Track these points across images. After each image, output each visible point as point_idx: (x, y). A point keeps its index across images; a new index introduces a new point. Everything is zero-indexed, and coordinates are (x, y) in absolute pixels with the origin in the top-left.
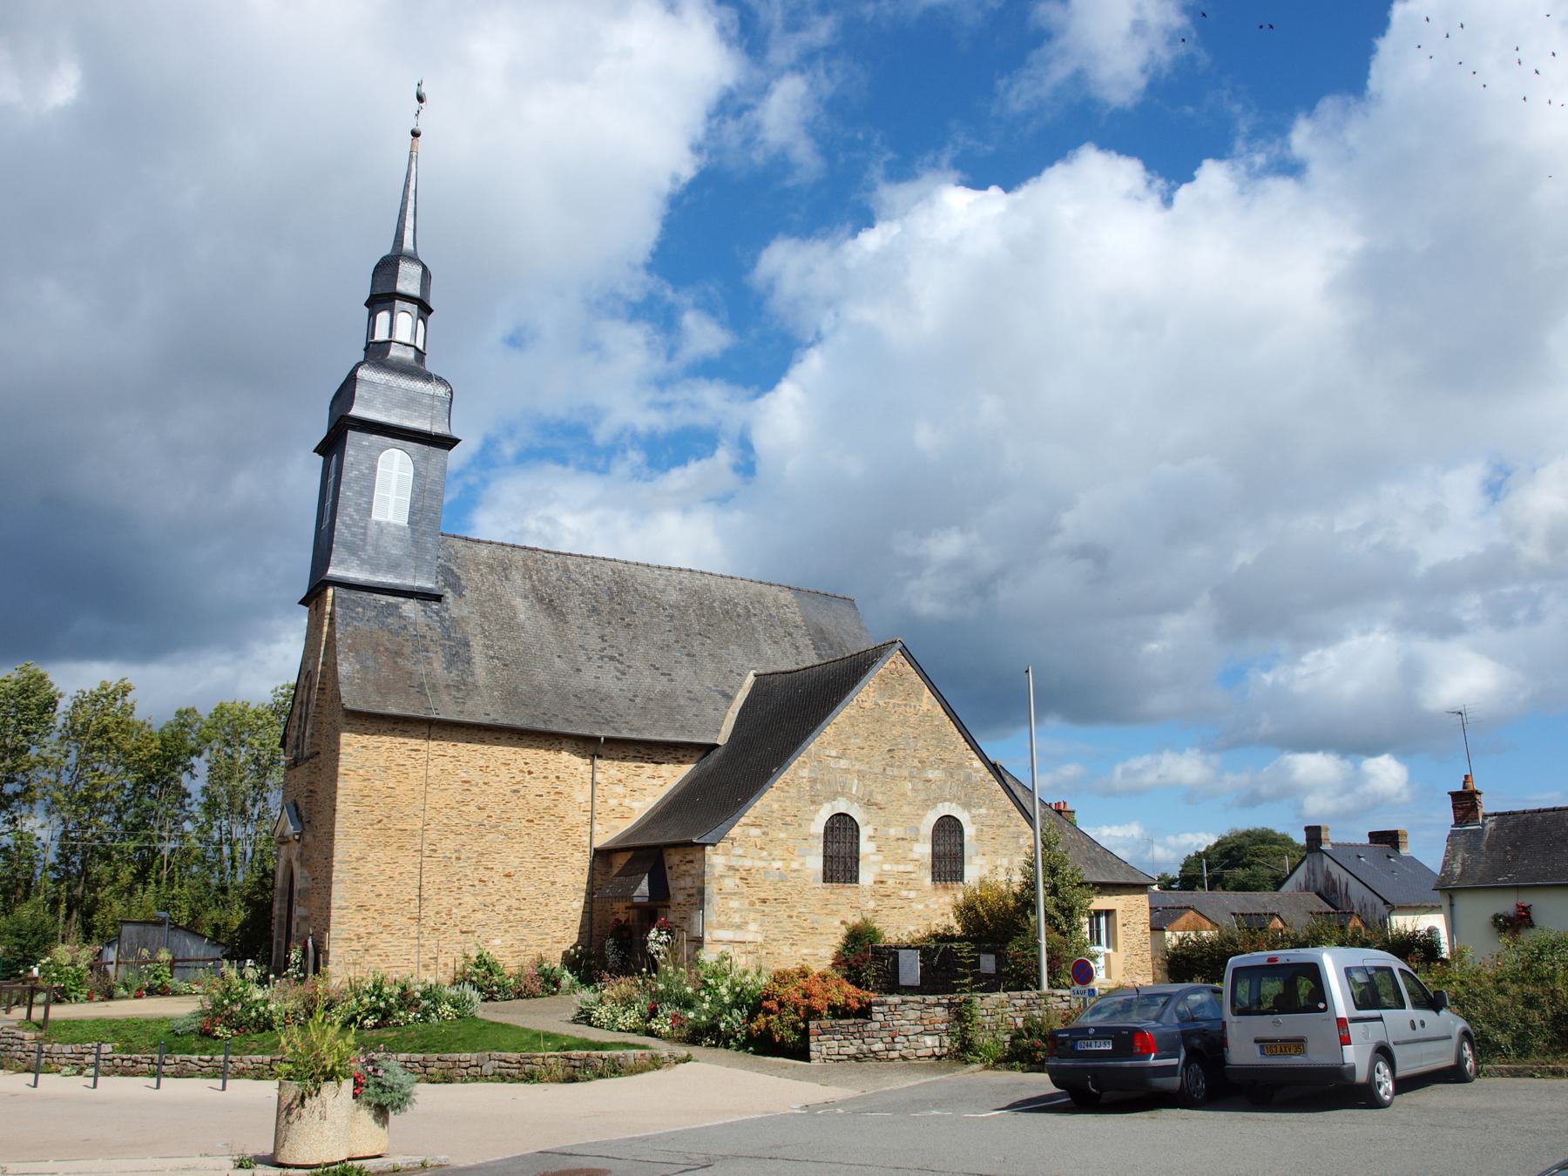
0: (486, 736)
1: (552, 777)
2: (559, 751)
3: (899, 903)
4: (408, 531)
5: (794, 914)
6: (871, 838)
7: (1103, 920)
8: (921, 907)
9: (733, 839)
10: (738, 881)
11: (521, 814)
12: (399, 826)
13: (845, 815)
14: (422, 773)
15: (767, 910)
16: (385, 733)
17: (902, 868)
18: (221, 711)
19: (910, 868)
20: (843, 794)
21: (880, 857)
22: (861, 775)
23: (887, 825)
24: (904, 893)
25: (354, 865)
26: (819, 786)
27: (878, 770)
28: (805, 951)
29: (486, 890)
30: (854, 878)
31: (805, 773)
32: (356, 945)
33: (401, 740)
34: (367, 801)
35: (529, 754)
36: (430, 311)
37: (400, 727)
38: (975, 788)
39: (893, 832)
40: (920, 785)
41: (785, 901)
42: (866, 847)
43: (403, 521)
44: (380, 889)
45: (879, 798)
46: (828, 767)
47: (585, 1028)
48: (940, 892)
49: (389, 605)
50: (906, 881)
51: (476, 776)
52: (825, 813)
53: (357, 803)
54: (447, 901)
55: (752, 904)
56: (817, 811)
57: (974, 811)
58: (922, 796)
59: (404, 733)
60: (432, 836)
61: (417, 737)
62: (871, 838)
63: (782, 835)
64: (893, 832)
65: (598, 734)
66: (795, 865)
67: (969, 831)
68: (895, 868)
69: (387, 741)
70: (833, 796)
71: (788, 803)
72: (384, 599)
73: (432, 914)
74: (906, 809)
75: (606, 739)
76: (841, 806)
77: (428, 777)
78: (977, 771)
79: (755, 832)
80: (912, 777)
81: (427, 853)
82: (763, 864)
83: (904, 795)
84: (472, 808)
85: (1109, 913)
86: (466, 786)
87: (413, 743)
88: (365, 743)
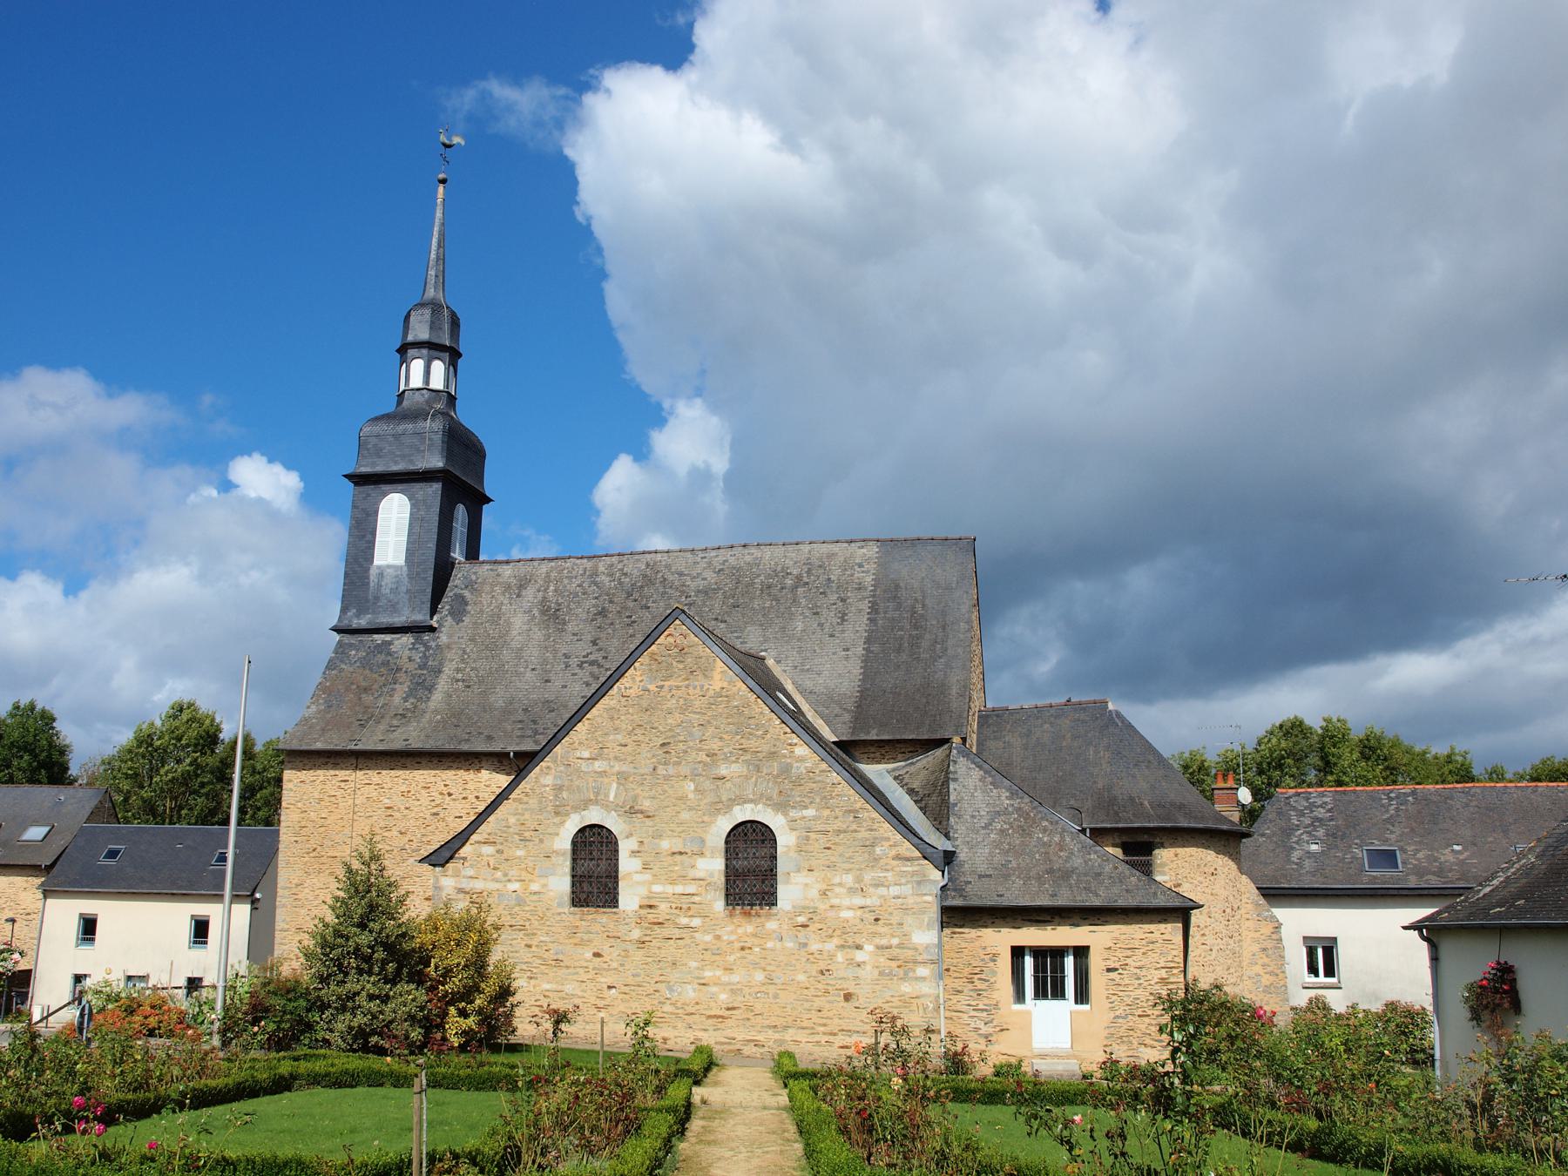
1: (471, 798)
2: (478, 770)
3: (677, 933)
5: (534, 943)
6: (634, 853)
7: (1069, 962)
8: (708, 938)
9: (464, 859)
13: (582, 830)
16: (319, 768)
17: (679, 889)
19: (691, 889)
20: (596, 802)
21: (647, 876)
22: (622, 778)
23: (658, 836)
24: (684, 921)
27: (649, 770)
28: (548, 986)
31: (548, 780)
33: (332, 772)
38: (798, 782)
39: (665, 845)
41: (523, 928)
42: (627, 864)
45: (646, 804)
46: (578, 770)
47: (485, 1056)
49: (384, 642)
50: (685, 904)
51: (399, 802)
56: (563, 823)
57: (793, 814)
58: (710, 798)
59: (336, 766)
61: (347, 769)
62: (634, 853)
63: (520, 853)
64: (665, 845)
65: (509, 749)
66: (535, 887)
67: (785, 840)
68: (670, 889)
69: (321, 774)
70: (585, 805)
71: (527, 816)
72: (379, 638)
74: (685, 815)
75: (516, 753)
76: (594, 816)
78: (801, 759)
79: (488, 850)
80: (694, 776)
83: (683, 798)
85: (1081, 952)
87: (343, 774)
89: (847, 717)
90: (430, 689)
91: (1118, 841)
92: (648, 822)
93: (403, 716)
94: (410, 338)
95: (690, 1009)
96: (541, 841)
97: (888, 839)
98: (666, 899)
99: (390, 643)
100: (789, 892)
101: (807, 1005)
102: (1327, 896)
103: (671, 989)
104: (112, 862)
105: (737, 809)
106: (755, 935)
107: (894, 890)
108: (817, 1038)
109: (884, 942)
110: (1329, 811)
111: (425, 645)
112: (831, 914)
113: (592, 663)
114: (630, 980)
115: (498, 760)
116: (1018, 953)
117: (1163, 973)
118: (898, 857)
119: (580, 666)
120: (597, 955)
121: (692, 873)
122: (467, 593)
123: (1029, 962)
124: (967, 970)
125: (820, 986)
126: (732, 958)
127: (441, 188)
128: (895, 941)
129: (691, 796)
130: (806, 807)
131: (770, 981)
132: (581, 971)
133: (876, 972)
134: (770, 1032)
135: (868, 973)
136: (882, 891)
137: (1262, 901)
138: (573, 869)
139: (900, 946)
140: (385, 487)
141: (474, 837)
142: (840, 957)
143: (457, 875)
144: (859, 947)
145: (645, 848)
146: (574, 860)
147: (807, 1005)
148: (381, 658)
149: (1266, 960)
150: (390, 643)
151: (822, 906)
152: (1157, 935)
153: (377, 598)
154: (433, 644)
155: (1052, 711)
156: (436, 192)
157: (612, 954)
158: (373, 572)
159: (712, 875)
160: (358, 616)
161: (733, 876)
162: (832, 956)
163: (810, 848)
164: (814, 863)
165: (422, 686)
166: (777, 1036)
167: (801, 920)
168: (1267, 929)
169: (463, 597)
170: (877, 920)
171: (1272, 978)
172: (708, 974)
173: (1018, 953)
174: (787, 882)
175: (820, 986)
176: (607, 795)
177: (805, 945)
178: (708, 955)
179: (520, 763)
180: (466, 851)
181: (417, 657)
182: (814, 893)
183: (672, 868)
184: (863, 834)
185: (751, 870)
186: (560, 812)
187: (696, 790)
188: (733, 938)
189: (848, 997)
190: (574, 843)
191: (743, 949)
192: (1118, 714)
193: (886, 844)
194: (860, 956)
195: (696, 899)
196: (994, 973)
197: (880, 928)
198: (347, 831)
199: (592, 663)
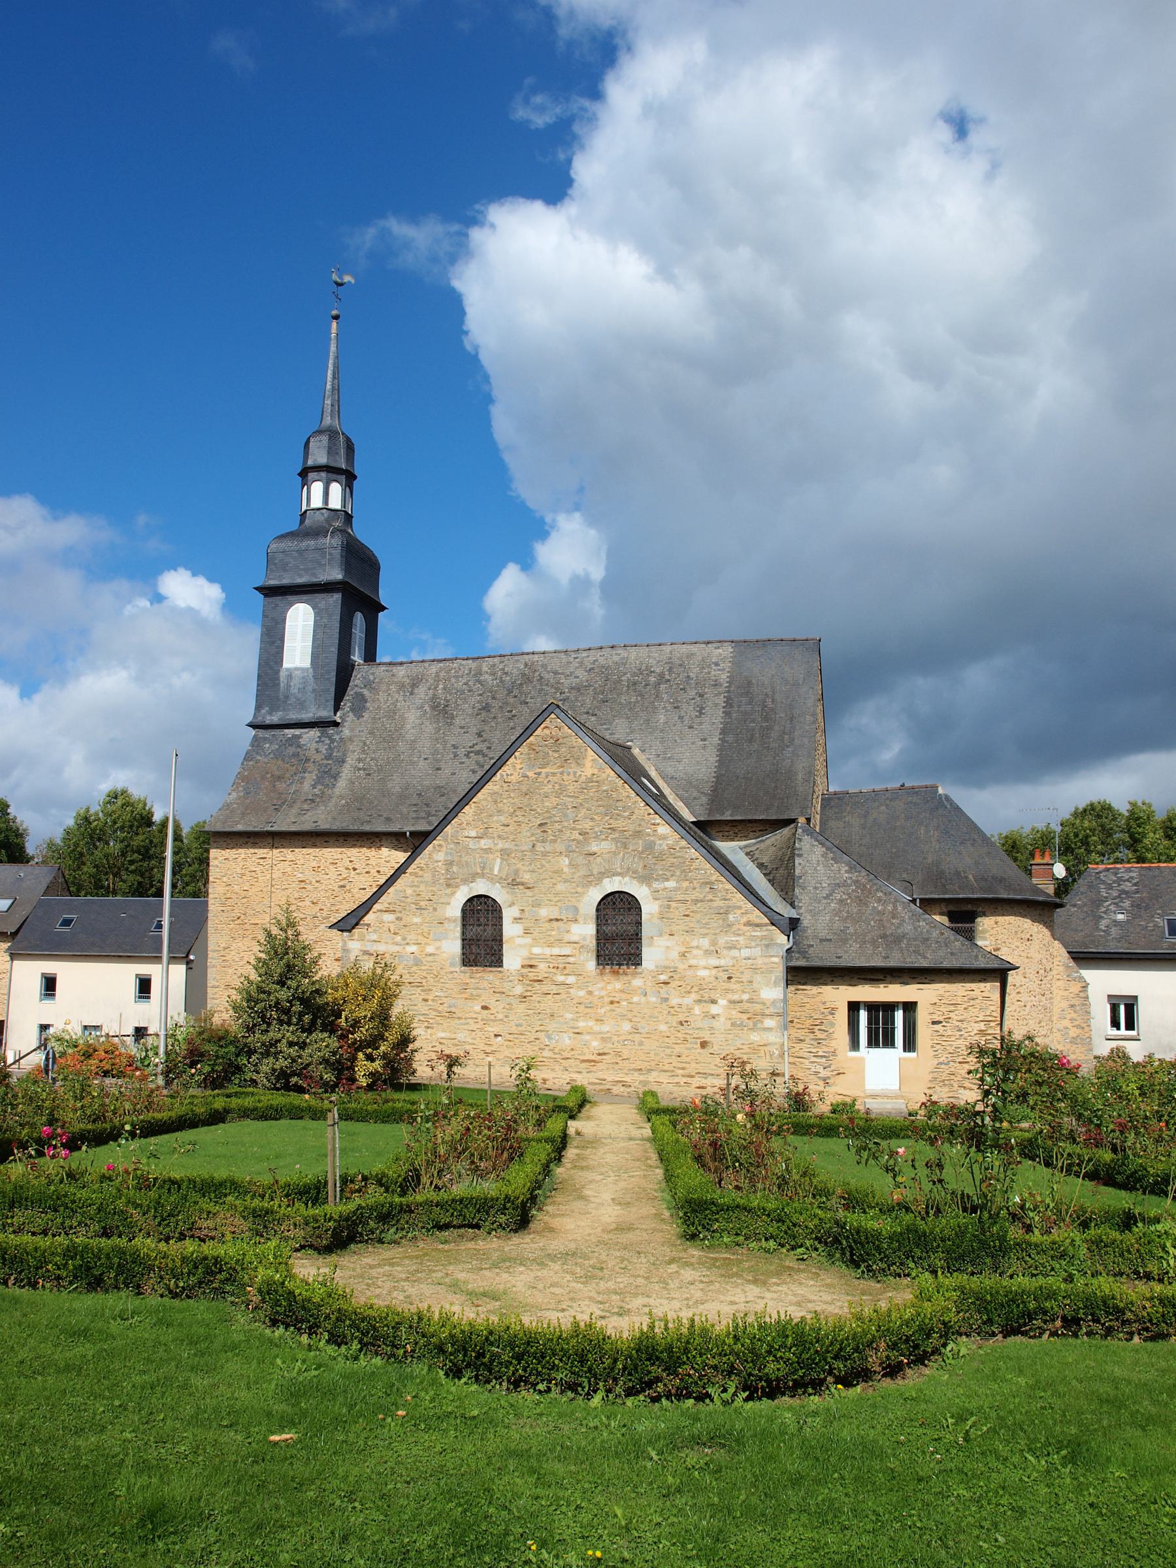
0: (318, 841)
1: (373, 872)
2: (379, 848)
3: (554, 989)
6: (517, 920)
7: (899, 1015)
9: (368, 925)
13: (470, 900)
16: (241, 847)
20: (483, 876)
21: (528, 940)
22: (505, 853)
24: (560, 978)
25: (222, 953)
26: (455, 869)
27: (528, 847)
28: (442, 1035)
30: (634, 959)
31: (440, 856)
33: (252, 851)
34: (229, 902)
35: (353, 853)
36: (355, 477)
37: (252, 840)
38: (660, 857)
39: (544, 912)
40: (581, 860)
41: (420, 985)
42: (510, 929)
45: (526, 877)
46: (467, 848)
47: (390, 1094)
49: (294, 736)
50: (562, 965)
51: (309, 875)
52: (462, 895)
53: (223, 904)
56: (453, 893)
57: (656, 885)
58: (583, 871)
62: (517, 920)
63: (417, 920)
64: (544, 912)
66: (430, 949)
67: (649, 909)
68: (548, 951)
69: (242, 852)
70: (472, 878)
71: (422, 887)
72: (289, 732)
74: (560, 887)
75: (412, 833)
77: (272, 879)
78: (664, 838)
80: (569, 852)
82: (397, 948)
83: (559, 872)
85: (910, 1007)
86: (303, 885)
87: (261, 852)
88: (227, 856)
89: (704, 800)
93: (312, 801)
94: (310, 463)
95: (566, 1055)
96: (435, 909)
98: (544, 960)
99: (299, 737)
100: (652, 954)
101: (668, 1051)
103: (549, 1038)
104: (66, 929)
105: (606, 881)
106: (622, 991)
107: (745, 953)
108: (676, 1080)
109: (736, 997)
110: (1135, 885)
111: (330, 738)
112: (689, 973)
113: (477, 753)
114: (514, 1030)
115: (396, 839)
116: (854, 1007)
117: (982, 1026)
118: (748, 924)
119: (467, 756)
120: (485, 1008)
121: (567, 937)
122: (366, 692)
123: (863, 1015)
124: (809, 1022)
125: (679, 1035)
126: (603, 1011)
127: (334, 324)
128: (745, 997)
130: (667, 880)
131: (636, 1030)
133: (729, 1022)
134: (636, 1074)
135: (721, 1024)
137: (1072, 964)
138: (463, 933)
139: (750, 1001)
140: (290, 598)
141: (376, 907)
142: (697, 1010)
144: (714, 1002)
145: (527, 915)
146: (464, 926)
147: (668, 1051)
148: (291, 750)
149: (1074, 1015)
150: (299, 737)
151: (681, 966)
153: (287, 697)
154: (337, 737)
155: (888, 795)
157: (497, 1007)
158: (283, 674)
159: (584, 939)
161: (602, 939)
162: (690, 1010)
163: (669, 915)
164: (674, 928)
165: (328, 775)
167: (663, 978)
168: (1075, 988)
169: (363, 695)
170: (730, 978)
171: (1079, 1031)
172: (581, 1024)
173: (854, 1007)
174: (651, 945)
175: (679, 1035)
176: (492, 869)
177: (667, 1000)
178: (581, 1008)
179: (416, 842)
180: (370, 918)
182: (674, 954)
183: (549, 933)
184: (719, 903)
185: (619, 934)
188: (604, 993)
189: (704, 1045)
190: (464, 911)
191: (612, 1003)
192: (947, 798)
193: (739, 912)
194: (714, 1010)
195: (571, 960)
196: (832, 1025)
197: (732, 985)
198: (266, 902)
199: (477, 753)
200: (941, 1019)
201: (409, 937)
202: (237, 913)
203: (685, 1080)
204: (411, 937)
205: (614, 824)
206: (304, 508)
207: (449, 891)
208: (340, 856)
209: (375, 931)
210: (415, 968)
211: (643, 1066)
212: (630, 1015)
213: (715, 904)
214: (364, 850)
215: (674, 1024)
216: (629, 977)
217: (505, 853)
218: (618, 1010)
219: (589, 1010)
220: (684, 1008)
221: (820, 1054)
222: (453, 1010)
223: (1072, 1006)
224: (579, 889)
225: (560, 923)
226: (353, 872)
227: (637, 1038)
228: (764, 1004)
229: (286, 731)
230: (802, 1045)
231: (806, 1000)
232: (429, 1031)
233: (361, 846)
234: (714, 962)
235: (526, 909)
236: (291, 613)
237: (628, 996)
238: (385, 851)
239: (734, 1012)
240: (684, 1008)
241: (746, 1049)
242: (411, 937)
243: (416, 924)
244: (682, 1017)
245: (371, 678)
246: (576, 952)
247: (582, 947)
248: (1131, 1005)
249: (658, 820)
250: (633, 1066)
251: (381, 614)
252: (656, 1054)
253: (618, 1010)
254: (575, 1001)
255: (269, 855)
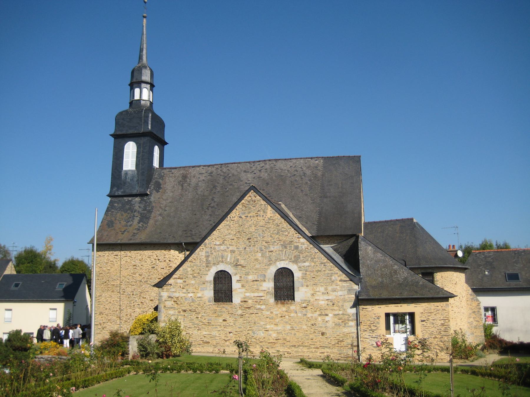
1: (167, 261)
2: (170, 250)
3: (256, 311)
4: (136, 171)
5: (199, 316)
9: (171, 285)
10: (173, 303)
11: (155, 276)
12: (112, 284)
14: (119, 263)
15: (186, 315)
17: (256, 294)
18: (25, 251)
19: (261, 294)
20: (222, 262)
21: (244, 290)
23: (247, 274)
24: (258, 307)
28: (205, 333)
29: (144, 306)
30: (292, 298)
32: (99, 327)
33: (112, 252)
34: (101, 275)
35: (158, 252)
38: (301, 252)
41: (195, 311)
42: (235, 285)
43: (134, 168)
44: (107, 307)
45: (242, 262)
48: (280, 305)
50: (259, 300)
51: (138, 263)
52: (213, 271)
54: (130, 311)
55: (179, 312)
56: (209, 270)
57: (299, 264)
59: (113, 250)
60: (123, 286)
63: (193, 282)
66: (199, 295)
67: (297, 275)
68: (252, 295)
71: (195, 268)
73: (125, 315)
75: (185, 244)
76: (221, 267)
79: (180, 281)
81: (122, 293)
83: (256, 260)
84: (137, 275)
85: (493, 309)
89: (315, 227)
90: (148, 218)
91: (420, 272)
92: (243, 269)
93: (139, 230)
94: (134, 80)
95: (261, 340)
96: (201, 277)
97: (337, 273)
98: (251, 298)
99: (131, 201)
100: (299, 295)
101: (307, 337)
102: (488, 291)
103: (254, 333)
104: (16, 289)
105: (278, 263)
106: (286, 311)
107: (340, 293)
108: (311, 350)
109: (337, 312)
110: (492, 259)
111: (145, 201)
112: (315, 303)
113: (212, 207)
114: (238, 330)
115: (179, 246)
116: (387, 315)
117: (442, 322)
118: (341, 281)
119: (208, 209)
120: (224, 320)
121: (261, 288)
122: (161, 181)
123: (392, 318)
124: (369, 322)
125: (312, 330)
126: (278, 320)
127: (145, 20)
128: (341, 312)
129: (260, 259)
130: (305, 262)
131: (293, 329)
132: (218, 327)
133: (334, 324)
134: (293, 348)
135: (330, 324)
136: (335, 293)
137: (473, 293)
138: (214, 287)
139: (343, 314)
140: (126, 139)
141: (174, 276)
142: (320, 319)
143: (168, 291)
144: (327, 315)
145: (242, 279)
146: (215, 284)
147: (307, 337)
148: (128, 207)
149: (474, 316)
150: (131, 201)
151: (312, 300)
152: (440, 307)
153: (125, 183)
154: (148, 201)
155: (392, 223)
156: (143, 21)
157: (230, 320)
158: (123, 173)
159: (269, 289)
160: (118, 190)
161: (277, 289)
162: (316, 319)
163: (306, 278)
164: (309, 283)
165: (144, 218)
166: (296, 349)
167: (304, 305)
168: (475, 304)
169: (159, 182)
170: (333, 304)
171: (477, 323)
172: (268, 327)
173: (387, 315)
174: (298, 291)
175: (312, 330)
176: (226, 259)
177: (306, 315)
178: (268, 320)
179: (190, 247)
180: (171, 281)
181: (142, 206)
182: (309, 295)
183: (253, 287)
184: (327, 272)
185: (284, 287)
186: (208, 265)
187: (262, 256)
188: (277, 313)
189: (323, 334)
190: (215, 278)
191: (282, 317)
192: (417, 223)
193: (336, 276)
194: (327, 318)
195: (263, 298)
196: (378, 323)
197: (335, 308)
198: (118, 275)
199: (212, 207)
200: (425, 319)
201: (189, 290)
202: (104, 280)
203: (315, 350)
204: (191, 289)
205: (281, 238)
206: (132, 99)
207: (207, 269)
208: (152, 254)
209: (174, 287)
210: (192, 304)
211: (297, 344)
212: (289, 323)
213: (326, 272)
214: (163, 251)
215: (310, 325)
216: (289, 305)
217: (233, 252)
218: (284, 320)
219: (271, 320)
220: (314, 318)
221: (374, 336)
222: (210, 322)
223: (474, 312)
224: (266, 267)
225: (257, 282)
226: (158, 261)
227: (293, 332)
228: (349, 315)
229: (125, 198)
230: (365, 333)
231: (367, 313)
232: (199, 331)
233: (162, 249)
234: (326, 297)
235: (242, 276)
236: (126, 146)
237: (289, 314)
238: (172, 251)
239: (336, 319)
240: (314, 318)
241: (341, 335)
242: (191, 289)
243: (192, 284)
244: (313, 322)
245: (163, 174)
246: (265, 295)
247: (268, 292)
248: (493, 309)
249: (300, 236)
250: (291, 344)
251: (165, 146)
252: (302, 339)
253: (284, 320)
254: (265, 317)
255: (119, 254)
